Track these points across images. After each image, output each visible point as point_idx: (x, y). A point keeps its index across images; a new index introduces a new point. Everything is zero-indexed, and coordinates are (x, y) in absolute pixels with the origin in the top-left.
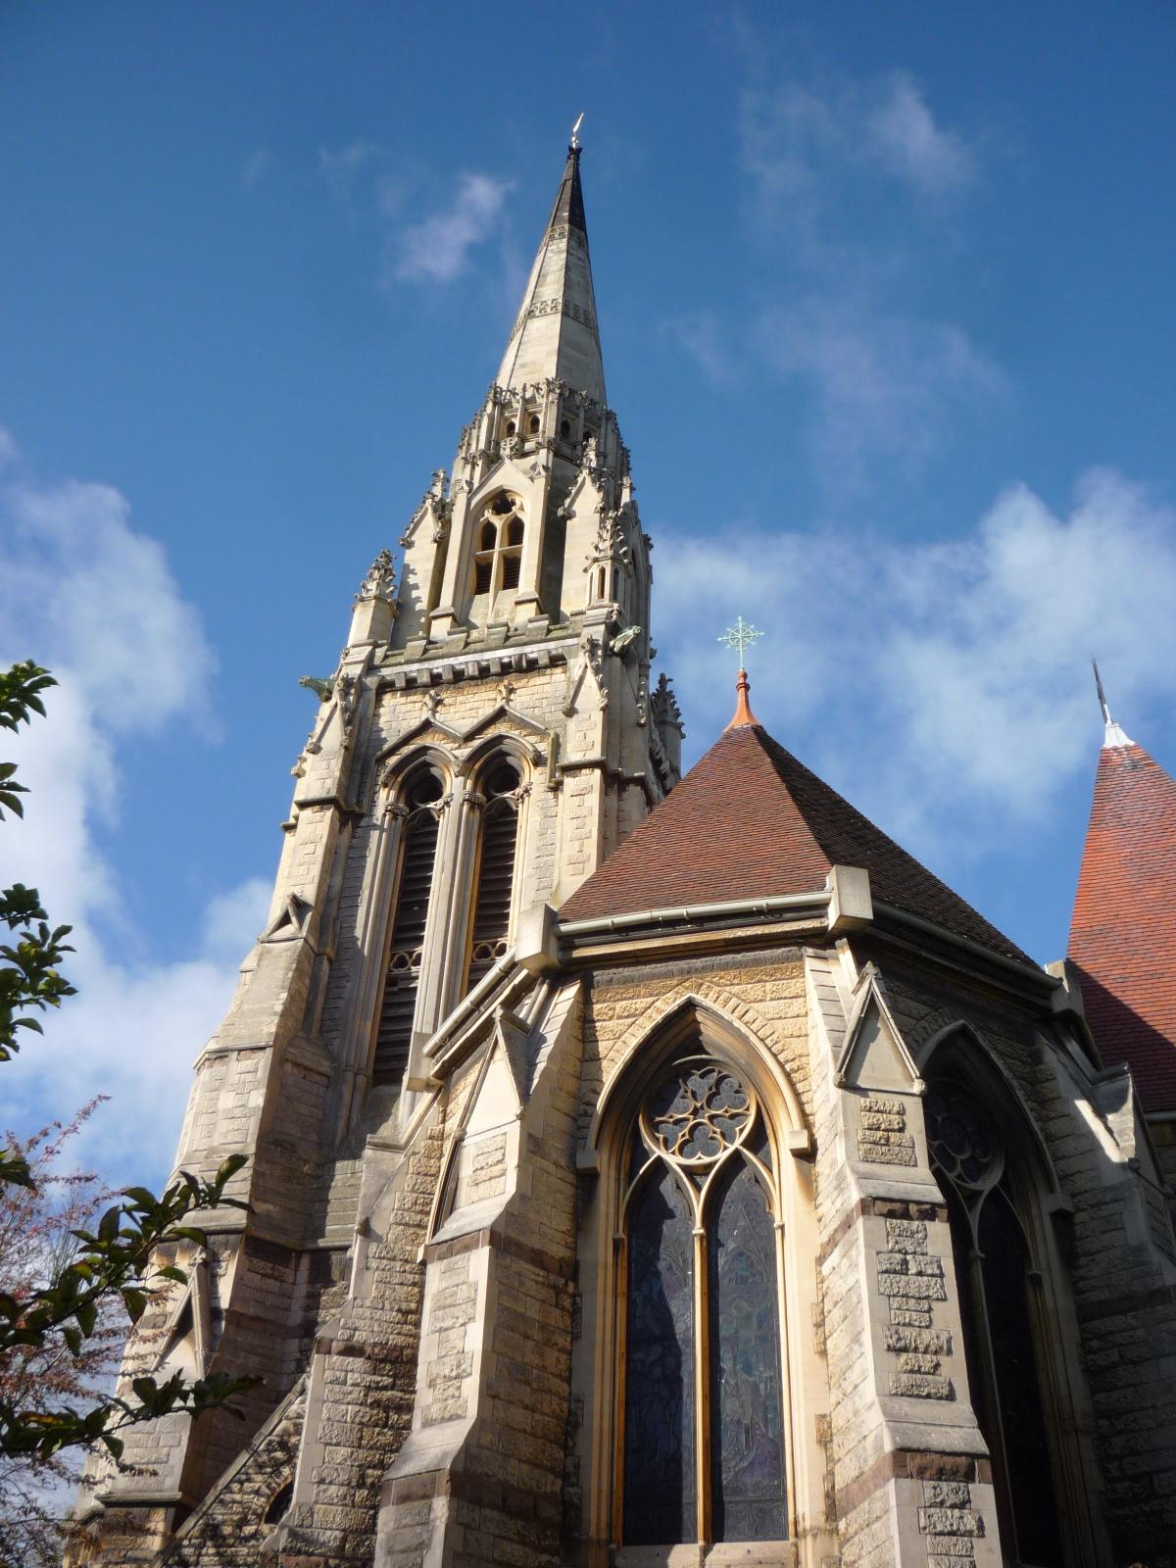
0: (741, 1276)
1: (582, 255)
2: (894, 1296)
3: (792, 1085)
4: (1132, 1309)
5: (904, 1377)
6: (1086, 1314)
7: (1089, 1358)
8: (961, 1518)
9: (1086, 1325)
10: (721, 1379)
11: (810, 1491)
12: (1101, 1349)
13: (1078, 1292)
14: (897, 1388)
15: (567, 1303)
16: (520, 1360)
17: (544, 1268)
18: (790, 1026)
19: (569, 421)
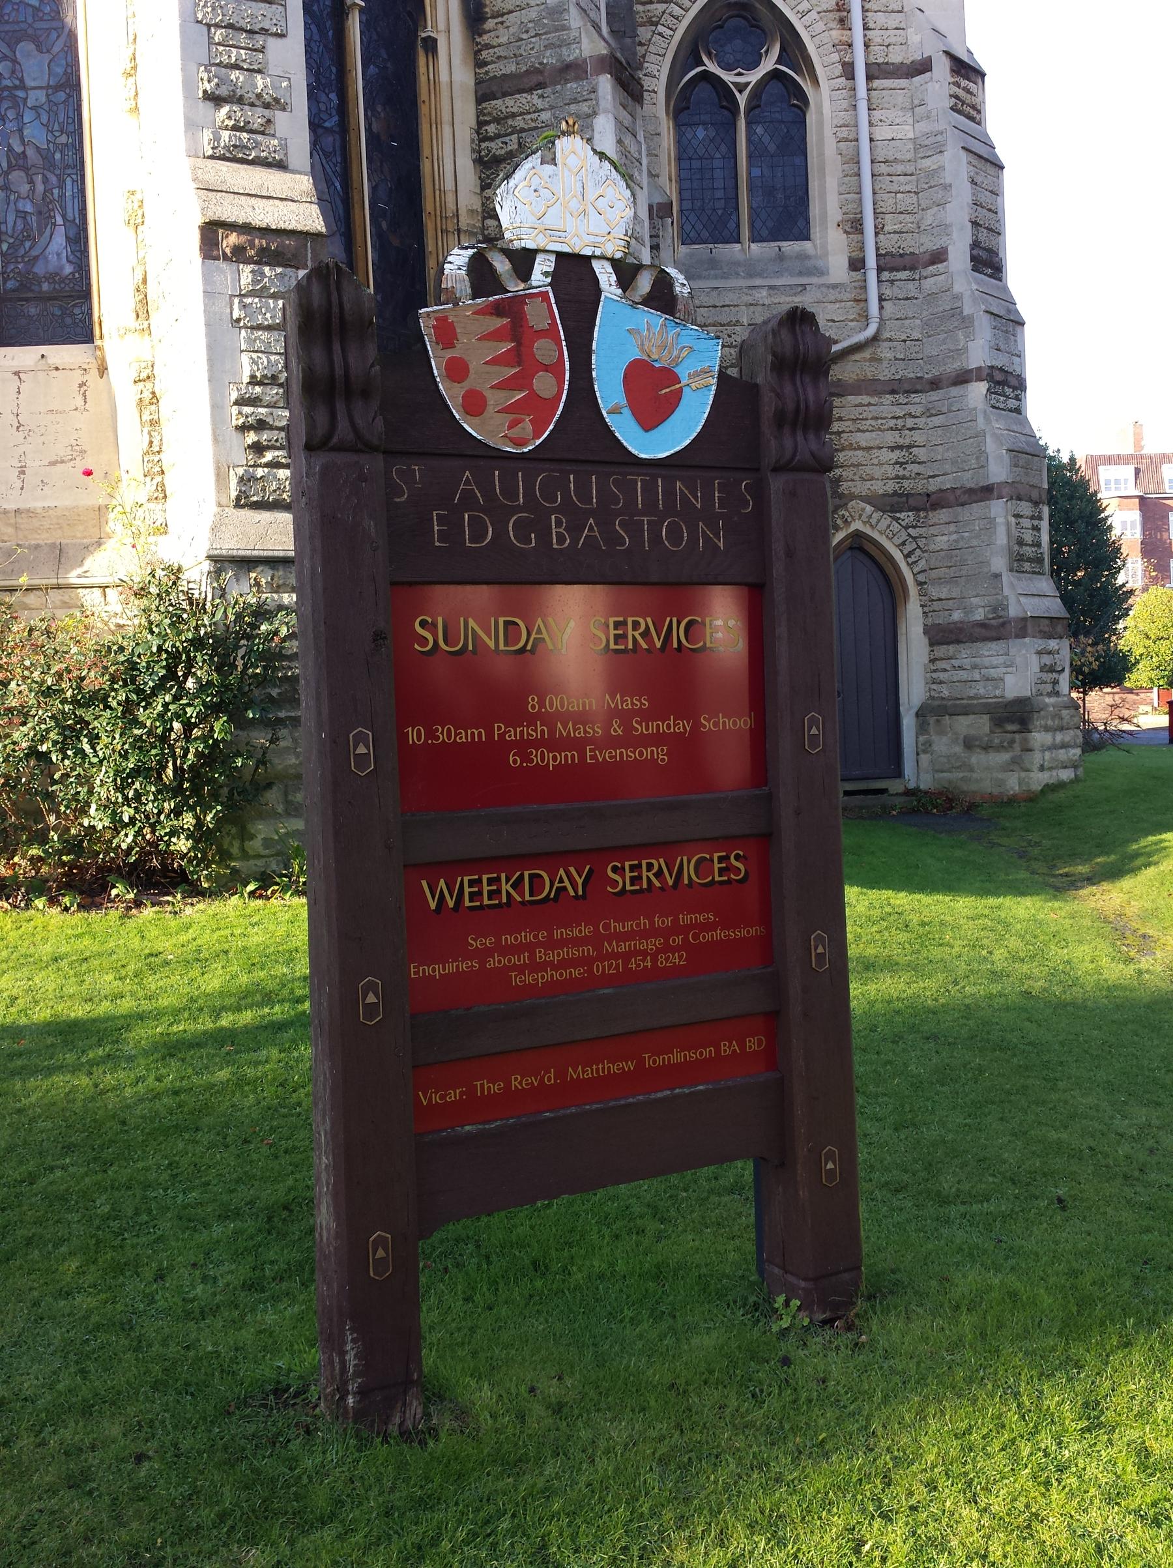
4: (541, 85)
6: (485, 92)
7: (483, 145)
9: (484, 105)
12: (498, 136)
13: (480, 64)
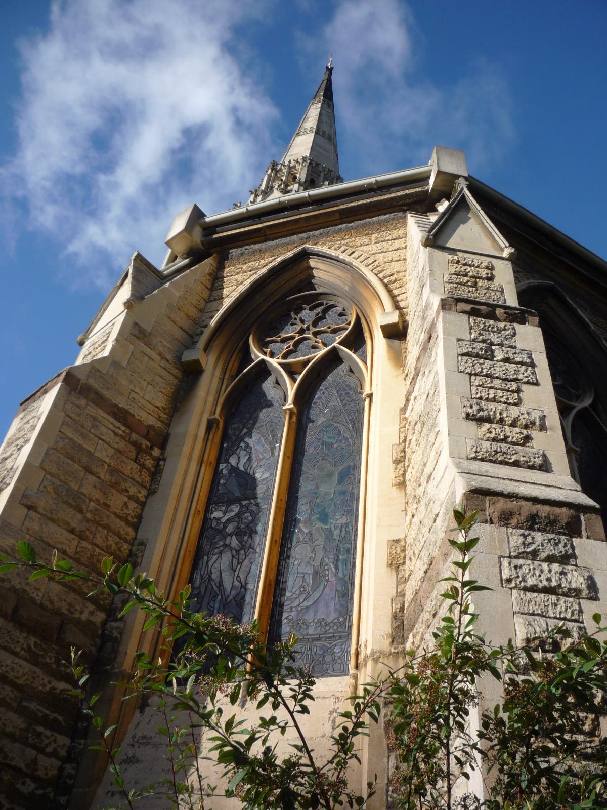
0: (328, 444)
1: (330, 111)
2: (476, 374)
3: (390, 291)
5: (486, 445)
8: (562, 573)
10: (295, 528)
11: (374, 614)
14: (476, 452)
15: (149, 463)
16: (76, 488)
17: (128, 427)
18: (395, 267)
19: (315, 178)
